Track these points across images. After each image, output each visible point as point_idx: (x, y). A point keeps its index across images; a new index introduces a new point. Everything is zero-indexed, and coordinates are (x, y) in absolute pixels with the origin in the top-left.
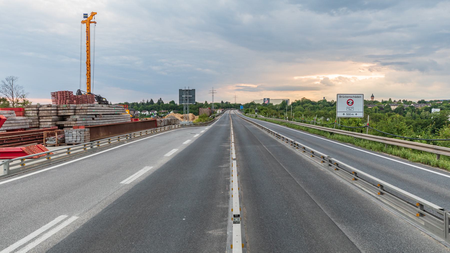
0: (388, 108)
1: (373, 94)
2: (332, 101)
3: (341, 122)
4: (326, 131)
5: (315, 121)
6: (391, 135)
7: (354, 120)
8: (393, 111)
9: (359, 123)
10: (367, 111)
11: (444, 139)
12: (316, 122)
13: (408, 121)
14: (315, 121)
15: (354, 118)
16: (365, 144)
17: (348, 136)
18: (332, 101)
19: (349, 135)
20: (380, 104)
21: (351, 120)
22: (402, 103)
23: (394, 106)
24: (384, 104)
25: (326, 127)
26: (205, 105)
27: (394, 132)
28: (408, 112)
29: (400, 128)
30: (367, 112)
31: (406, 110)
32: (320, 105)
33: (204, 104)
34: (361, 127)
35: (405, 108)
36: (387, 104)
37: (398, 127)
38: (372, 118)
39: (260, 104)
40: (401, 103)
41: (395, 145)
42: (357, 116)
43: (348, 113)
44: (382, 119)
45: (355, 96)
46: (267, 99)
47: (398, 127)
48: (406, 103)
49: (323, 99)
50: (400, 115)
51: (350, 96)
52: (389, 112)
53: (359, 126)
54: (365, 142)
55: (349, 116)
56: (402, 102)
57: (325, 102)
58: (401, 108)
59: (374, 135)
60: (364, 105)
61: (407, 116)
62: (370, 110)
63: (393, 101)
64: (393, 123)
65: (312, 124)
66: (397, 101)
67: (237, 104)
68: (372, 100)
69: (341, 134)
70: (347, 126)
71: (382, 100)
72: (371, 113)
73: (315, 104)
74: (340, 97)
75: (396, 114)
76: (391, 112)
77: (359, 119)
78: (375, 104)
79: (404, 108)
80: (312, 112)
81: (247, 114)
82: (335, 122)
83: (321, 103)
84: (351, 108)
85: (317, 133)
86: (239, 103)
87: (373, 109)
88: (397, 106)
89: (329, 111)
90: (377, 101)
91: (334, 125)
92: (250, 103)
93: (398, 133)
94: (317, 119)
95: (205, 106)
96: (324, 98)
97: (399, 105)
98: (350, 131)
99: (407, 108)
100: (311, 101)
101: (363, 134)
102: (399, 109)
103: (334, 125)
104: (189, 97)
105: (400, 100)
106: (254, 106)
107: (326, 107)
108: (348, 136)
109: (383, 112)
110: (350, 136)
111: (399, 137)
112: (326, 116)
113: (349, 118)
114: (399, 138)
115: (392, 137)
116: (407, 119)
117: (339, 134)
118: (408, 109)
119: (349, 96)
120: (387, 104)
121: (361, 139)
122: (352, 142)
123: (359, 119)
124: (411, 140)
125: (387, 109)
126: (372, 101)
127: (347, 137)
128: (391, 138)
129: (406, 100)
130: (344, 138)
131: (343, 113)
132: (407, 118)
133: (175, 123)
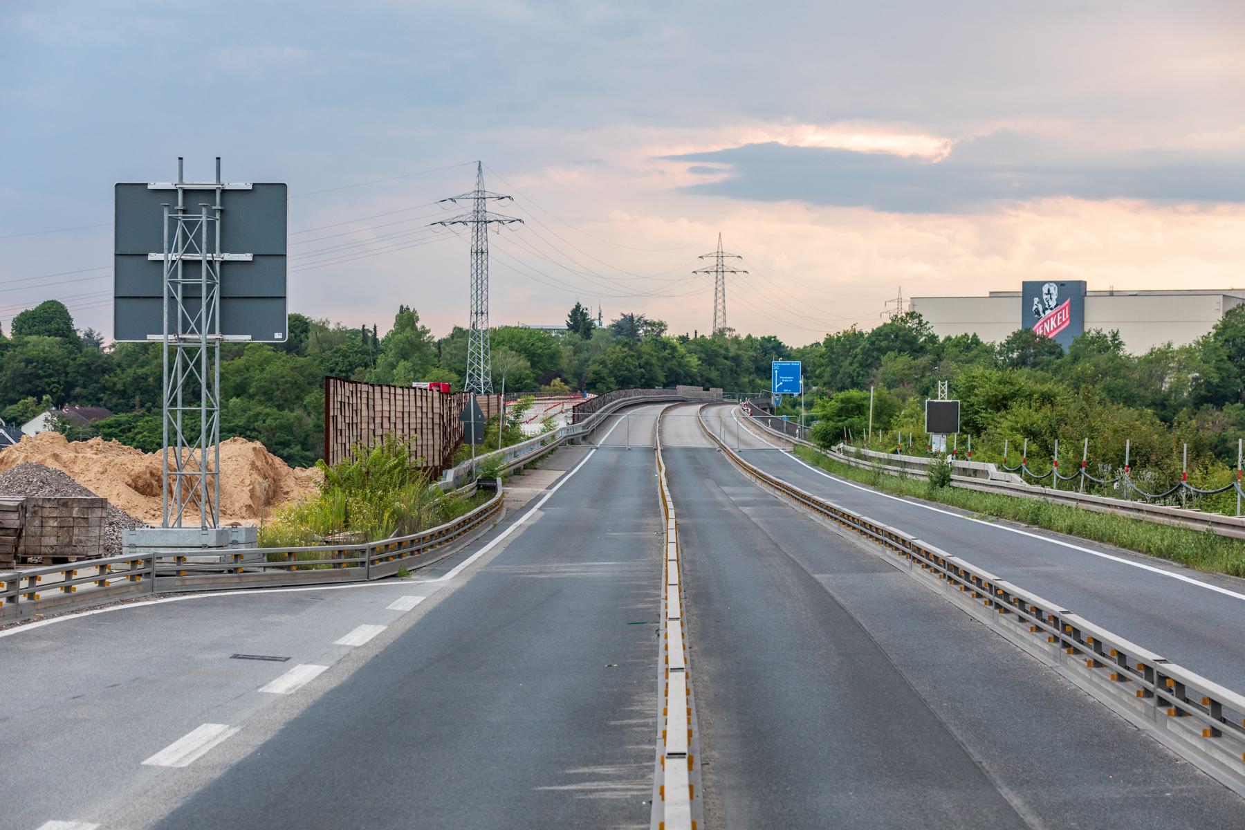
39: (985, 339)
46: (1061, 285)
81: (837, 453)
86: (758, 335)
92: (878, 334)
95: (393, 366)
104: (223, 263)
106: (924, 360)
133: (69, 544)
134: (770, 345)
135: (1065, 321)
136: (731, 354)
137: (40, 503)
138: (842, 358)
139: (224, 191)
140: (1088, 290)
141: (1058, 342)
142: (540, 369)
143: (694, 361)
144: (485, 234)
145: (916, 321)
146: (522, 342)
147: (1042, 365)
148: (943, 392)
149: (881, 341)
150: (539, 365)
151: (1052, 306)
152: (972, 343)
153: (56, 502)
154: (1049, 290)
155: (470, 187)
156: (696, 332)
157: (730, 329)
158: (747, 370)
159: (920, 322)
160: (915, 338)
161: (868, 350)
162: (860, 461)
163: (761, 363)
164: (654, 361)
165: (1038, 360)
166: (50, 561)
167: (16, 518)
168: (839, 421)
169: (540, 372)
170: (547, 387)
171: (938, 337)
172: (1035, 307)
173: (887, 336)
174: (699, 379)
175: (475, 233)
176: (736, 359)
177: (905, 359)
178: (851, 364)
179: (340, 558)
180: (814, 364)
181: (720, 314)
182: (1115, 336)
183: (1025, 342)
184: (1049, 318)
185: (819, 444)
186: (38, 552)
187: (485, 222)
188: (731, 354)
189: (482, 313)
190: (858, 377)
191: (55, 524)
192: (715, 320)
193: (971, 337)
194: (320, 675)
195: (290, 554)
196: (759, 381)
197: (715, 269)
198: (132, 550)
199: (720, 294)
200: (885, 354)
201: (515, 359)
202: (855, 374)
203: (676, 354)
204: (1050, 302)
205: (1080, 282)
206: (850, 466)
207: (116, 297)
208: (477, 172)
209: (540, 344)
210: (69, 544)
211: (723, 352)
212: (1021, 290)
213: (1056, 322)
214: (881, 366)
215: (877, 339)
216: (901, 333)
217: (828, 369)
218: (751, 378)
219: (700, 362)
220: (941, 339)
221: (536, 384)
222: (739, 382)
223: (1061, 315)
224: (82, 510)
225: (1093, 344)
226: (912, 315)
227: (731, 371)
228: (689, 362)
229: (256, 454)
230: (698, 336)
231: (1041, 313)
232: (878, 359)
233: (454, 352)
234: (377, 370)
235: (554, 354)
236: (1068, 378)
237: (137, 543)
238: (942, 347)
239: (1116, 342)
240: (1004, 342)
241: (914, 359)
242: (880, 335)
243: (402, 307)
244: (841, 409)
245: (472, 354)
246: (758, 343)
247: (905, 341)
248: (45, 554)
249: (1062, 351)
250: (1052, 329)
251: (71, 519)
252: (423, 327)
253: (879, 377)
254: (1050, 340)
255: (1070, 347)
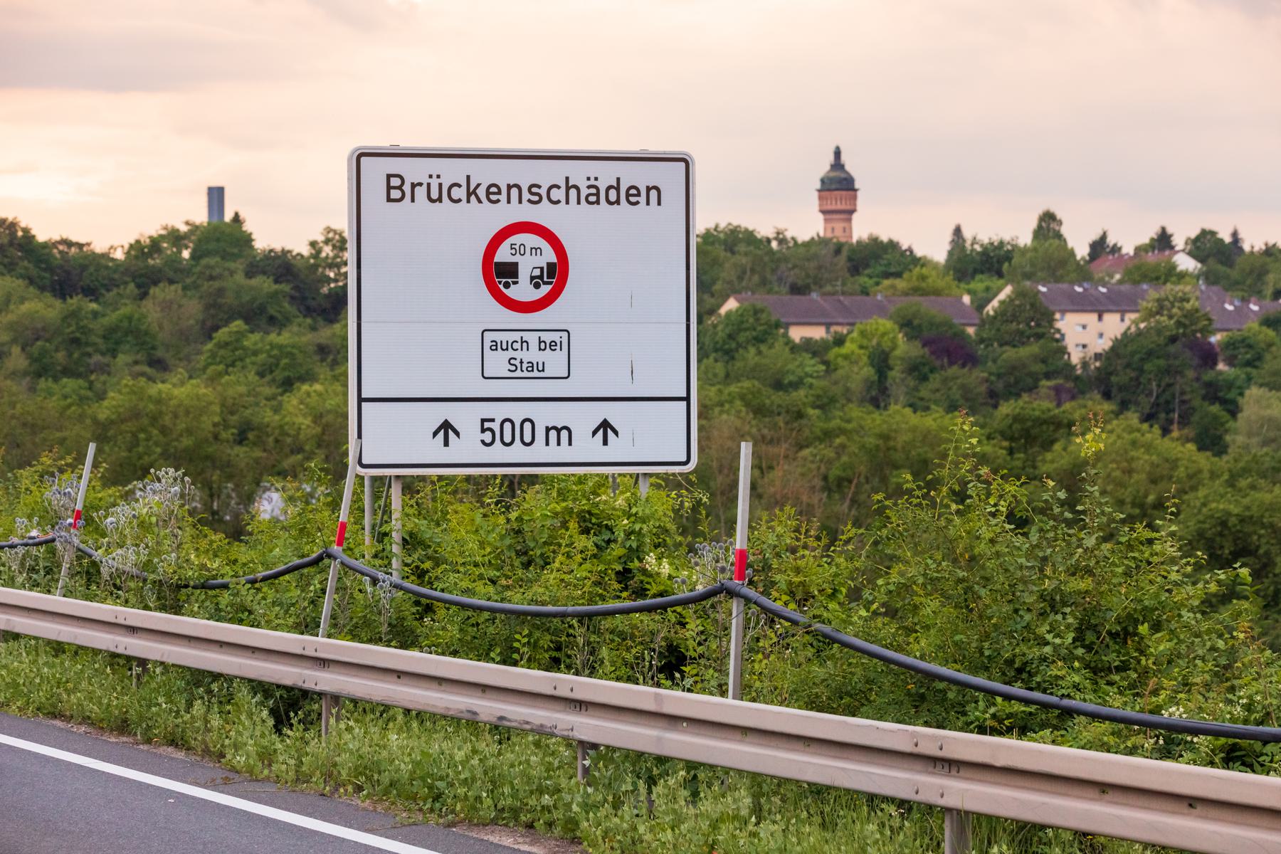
0: (1019, 339)
1: (838, 153)
2: (327, 251)
3: (411, 542)
4: (216, 676)
5: (71, 539)
6: (1008, 697)
7: (584, 505)
8: (1077, 378)
9: (637, 553)
10: (778, 385)
11: (1105, 710)
12: (81, 554)
13: (1255, 511)
14: (71, 539)
15: (581, 480)
16: (705, 825)
17: (502, 731)
18: (327, 251)
19: (517, 712)
20: (935, 281)
21: (537, 505)
22: (1182, 276)
23: (1091, 318)
24: (979, 284)
25: (217, 615)
27: (1043, 659)
28: (1254, 392)
29: (1118, 603)
30: (778, 398)
31: (1231, 362)
32: (167, 306)
33: (822, 234)
34: (664, 607)
35: (1215, 339)
36: (1008, 290)
37: (1085, 584)
38: (835, 472)
40: (1171, 274)
41: (1056, 828)
42: (618, 450)
43: (498, 411)
44: (909, 492)
45: (579, 173)
47: (1085, 584)
48: (1235, 274)
49: (201, 216)
50: (1166, 431)
51: (524, 174)
52: (1032, 389)
53: (641, 592)
54: (706, 806)
55: (518, 453)
56: (1186, 263)
57: (225, 256)
58: (1173, 339)
59: (814, 704)
61: (1240, 439)
62: (811, 365)
63: (1082, 251)
64: (1034, 537)
65: (35, 585)
66: (1128, 249)
68: (839, 235)
69: (407, 711)
70: (483, 595)
71: (958, 231)
72: (825, 404)
73: (91, 292)
74: (396, 190)
75: (1117, 414)
76: (1059, 395)
77: (644, 489)
78: (865, 292)
79: (1207, 331)
80: (53, 404)
82: (326, 545)
83: (173, 273)
84: (532, 338)
85: (94, 709)
87: (849, 347)
88: (1131, 317)
89: (288, 385)
90: (893, 245)
91: (316, 585)
93: (1097, 671)
94: (90, 507)
96: (216, 196)
97: (1152, 294)
98: (531, 662)
99: (1246, 343)
100: (28, 237)
101: (675, 699)
102: (1150, 354)
103: (316, 585)
105: (1163, 240)
107: (240, 335)
108: (495, 728)
109: (963, 387)
110: (523, 732)
111: (1094, 716)
112: (240, 451)
113: (514, 485)
114: (1107, 725)
115: (1023, 728)
116: (1243, 483)
117: (383, 711)
118: (1259, 358)
119: (502, 173)
120: (1008, 290)
121: (661, 760)
122: (546, 809)
123: (644, 489)
124: (1234, 748)
125: (1010, 354)
126: (838, 249)
127: (487, 745)
128: (1008, 731)
129: (1235, 235)
130: (452, 764)
131: (441, 412)
132: (1246, 471)
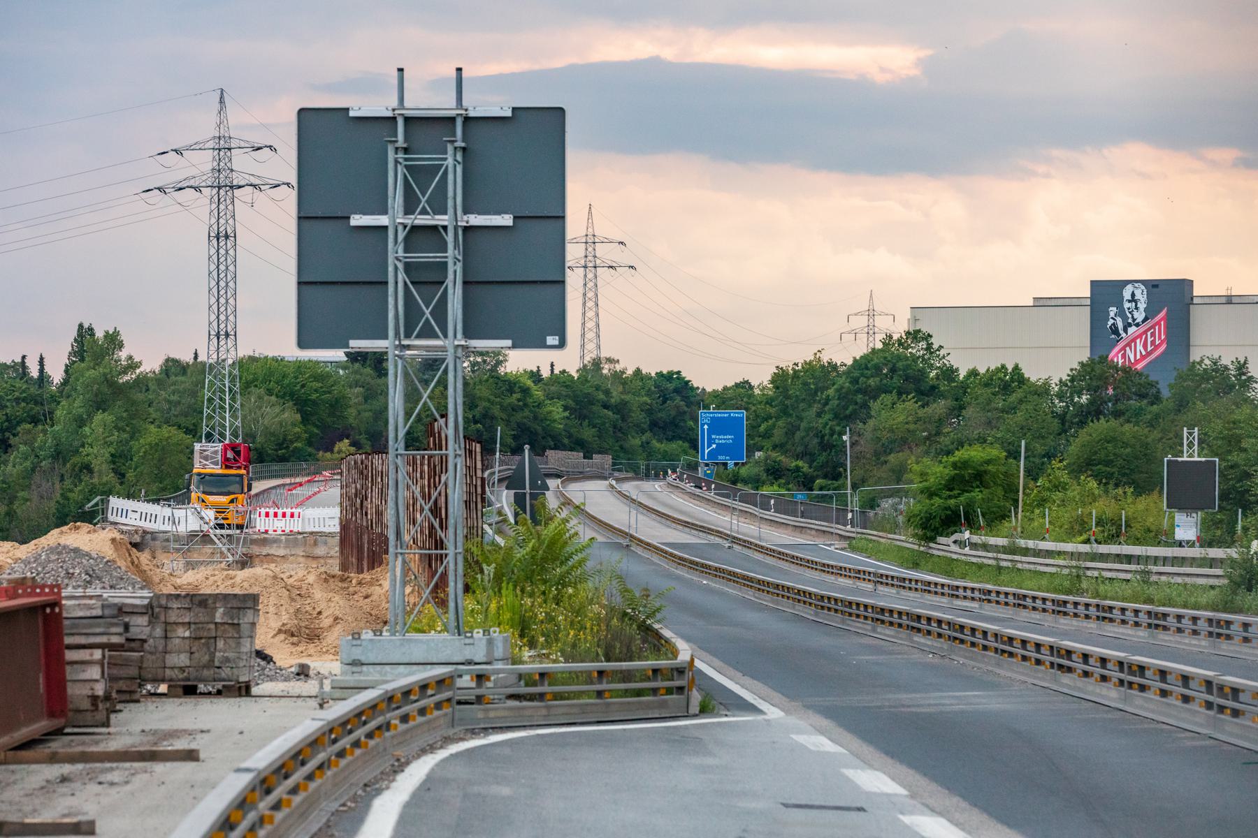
26: (78, 405)
39: (1034, 374)
46: (1153, 286)
60: (711, 495)
67: (618, 376)
81: (947, 546)
86: (651, 369)
92: (862, 365)
95: (81, 422)
104: (467, 229)
106: (940, 407)
133: (210, 665)
134: (671, 386)
135: (1160, 345)
136: (613, 400)
137: (163, 602)
138: (802, 405)
139: (467, 119)
140: (1194, 294)
141: (1152, 378)
142: (317, 427)
143: (556, 411)
144: (230, 207)
145: (923, 344)
146: (286, 381)
147: (1128, 414)
148: (1190, 445)
149: (868, 378)
150: (313, 418)
151: (1139, 319)
152: (1012, 380)
153: (188, 599)
154: (1133, 295)
155: (204, 126)
156: (552, 365)
157: (610, 360)
158: (637, 426)
159: (929, 346)
160: (923, 373)
161: (847, 393)
162: (1017, 558)
163: (660, 415)
164: (496, 411)
165: (1120, 406)
166: (180, 691)
167: (145, 624)
168: (950, 497)
169: (316, 431)
170: (328, 455)
171: (957, 370)
172: (1111, 322)
173: (878, 369)
174: (566, 441)
175: (214, 206)
176: (621, 409)
177: (910, 405)
178: (819, 415)
179: (600, 682)
180: (757, 416)
181: (590, 335)
182: (1242, 367)
183: (1100, 378)
184: (1134, 340)
185: (914, 536)
186: (160, 677)
187: (231, 187)
188: (613, 400)
189: (227, 335)
190: (832, 435)
191: (187, 634)
192: (583, 346)
193: (1010, 370)
194: (956, 825)
195: (542, 675)
196: (656, 444)
197: (582, 262)
198: (355, 669)
199: (590, 304)
200: (875, 398)
201: (277, 409)
202: (827, 431)
203: (530, 400)
204: (1136, 314)
205: (1184, 280)
206: (999, 568)
207: (299, 283)
208: (218, 106)
209: (316, 385)
210: (210, 665)
211: (601, 396)
212: (1089, 295)
213: (1145, 346)
214: (870, 417)
215: (862, 375)
216: (900, 365)
217: (780, 423)
218: (644, 438)
219: (567, 414)
220: (962, 374)
221: (310, 450)
222: (626, 445)
223: (1153, 335)
224: (230, 611)
225: (1208, 380)
226: (915, 335)
227: (615, 427)
228: (550, 412)
229: (116, 549)
230: (556, 371)
231: (1121, 332)
232: (865, 406)
233: (175, 398)
234: (56, 428)
235: (337, 401)
236: (1171, 435)
237: (363, 659)
238: (964, 387)
239: (1244, 377)
240: (1065, 378)
241: (923, 406)
242: (867, 368)
243: (81, 326)
244: (953, 479)
245: (210, 400)
246: (651, 383)
247: (907, 378)
248: (171, 680)
249: (1158, 392)
250: (1138, 357)
251: (212, 626)
252: (130, 358)
253: (868, 435)
254: (1139, 374)
255: (1171, 387)
